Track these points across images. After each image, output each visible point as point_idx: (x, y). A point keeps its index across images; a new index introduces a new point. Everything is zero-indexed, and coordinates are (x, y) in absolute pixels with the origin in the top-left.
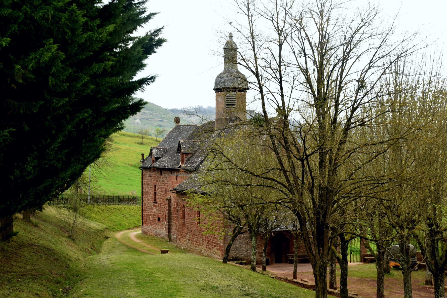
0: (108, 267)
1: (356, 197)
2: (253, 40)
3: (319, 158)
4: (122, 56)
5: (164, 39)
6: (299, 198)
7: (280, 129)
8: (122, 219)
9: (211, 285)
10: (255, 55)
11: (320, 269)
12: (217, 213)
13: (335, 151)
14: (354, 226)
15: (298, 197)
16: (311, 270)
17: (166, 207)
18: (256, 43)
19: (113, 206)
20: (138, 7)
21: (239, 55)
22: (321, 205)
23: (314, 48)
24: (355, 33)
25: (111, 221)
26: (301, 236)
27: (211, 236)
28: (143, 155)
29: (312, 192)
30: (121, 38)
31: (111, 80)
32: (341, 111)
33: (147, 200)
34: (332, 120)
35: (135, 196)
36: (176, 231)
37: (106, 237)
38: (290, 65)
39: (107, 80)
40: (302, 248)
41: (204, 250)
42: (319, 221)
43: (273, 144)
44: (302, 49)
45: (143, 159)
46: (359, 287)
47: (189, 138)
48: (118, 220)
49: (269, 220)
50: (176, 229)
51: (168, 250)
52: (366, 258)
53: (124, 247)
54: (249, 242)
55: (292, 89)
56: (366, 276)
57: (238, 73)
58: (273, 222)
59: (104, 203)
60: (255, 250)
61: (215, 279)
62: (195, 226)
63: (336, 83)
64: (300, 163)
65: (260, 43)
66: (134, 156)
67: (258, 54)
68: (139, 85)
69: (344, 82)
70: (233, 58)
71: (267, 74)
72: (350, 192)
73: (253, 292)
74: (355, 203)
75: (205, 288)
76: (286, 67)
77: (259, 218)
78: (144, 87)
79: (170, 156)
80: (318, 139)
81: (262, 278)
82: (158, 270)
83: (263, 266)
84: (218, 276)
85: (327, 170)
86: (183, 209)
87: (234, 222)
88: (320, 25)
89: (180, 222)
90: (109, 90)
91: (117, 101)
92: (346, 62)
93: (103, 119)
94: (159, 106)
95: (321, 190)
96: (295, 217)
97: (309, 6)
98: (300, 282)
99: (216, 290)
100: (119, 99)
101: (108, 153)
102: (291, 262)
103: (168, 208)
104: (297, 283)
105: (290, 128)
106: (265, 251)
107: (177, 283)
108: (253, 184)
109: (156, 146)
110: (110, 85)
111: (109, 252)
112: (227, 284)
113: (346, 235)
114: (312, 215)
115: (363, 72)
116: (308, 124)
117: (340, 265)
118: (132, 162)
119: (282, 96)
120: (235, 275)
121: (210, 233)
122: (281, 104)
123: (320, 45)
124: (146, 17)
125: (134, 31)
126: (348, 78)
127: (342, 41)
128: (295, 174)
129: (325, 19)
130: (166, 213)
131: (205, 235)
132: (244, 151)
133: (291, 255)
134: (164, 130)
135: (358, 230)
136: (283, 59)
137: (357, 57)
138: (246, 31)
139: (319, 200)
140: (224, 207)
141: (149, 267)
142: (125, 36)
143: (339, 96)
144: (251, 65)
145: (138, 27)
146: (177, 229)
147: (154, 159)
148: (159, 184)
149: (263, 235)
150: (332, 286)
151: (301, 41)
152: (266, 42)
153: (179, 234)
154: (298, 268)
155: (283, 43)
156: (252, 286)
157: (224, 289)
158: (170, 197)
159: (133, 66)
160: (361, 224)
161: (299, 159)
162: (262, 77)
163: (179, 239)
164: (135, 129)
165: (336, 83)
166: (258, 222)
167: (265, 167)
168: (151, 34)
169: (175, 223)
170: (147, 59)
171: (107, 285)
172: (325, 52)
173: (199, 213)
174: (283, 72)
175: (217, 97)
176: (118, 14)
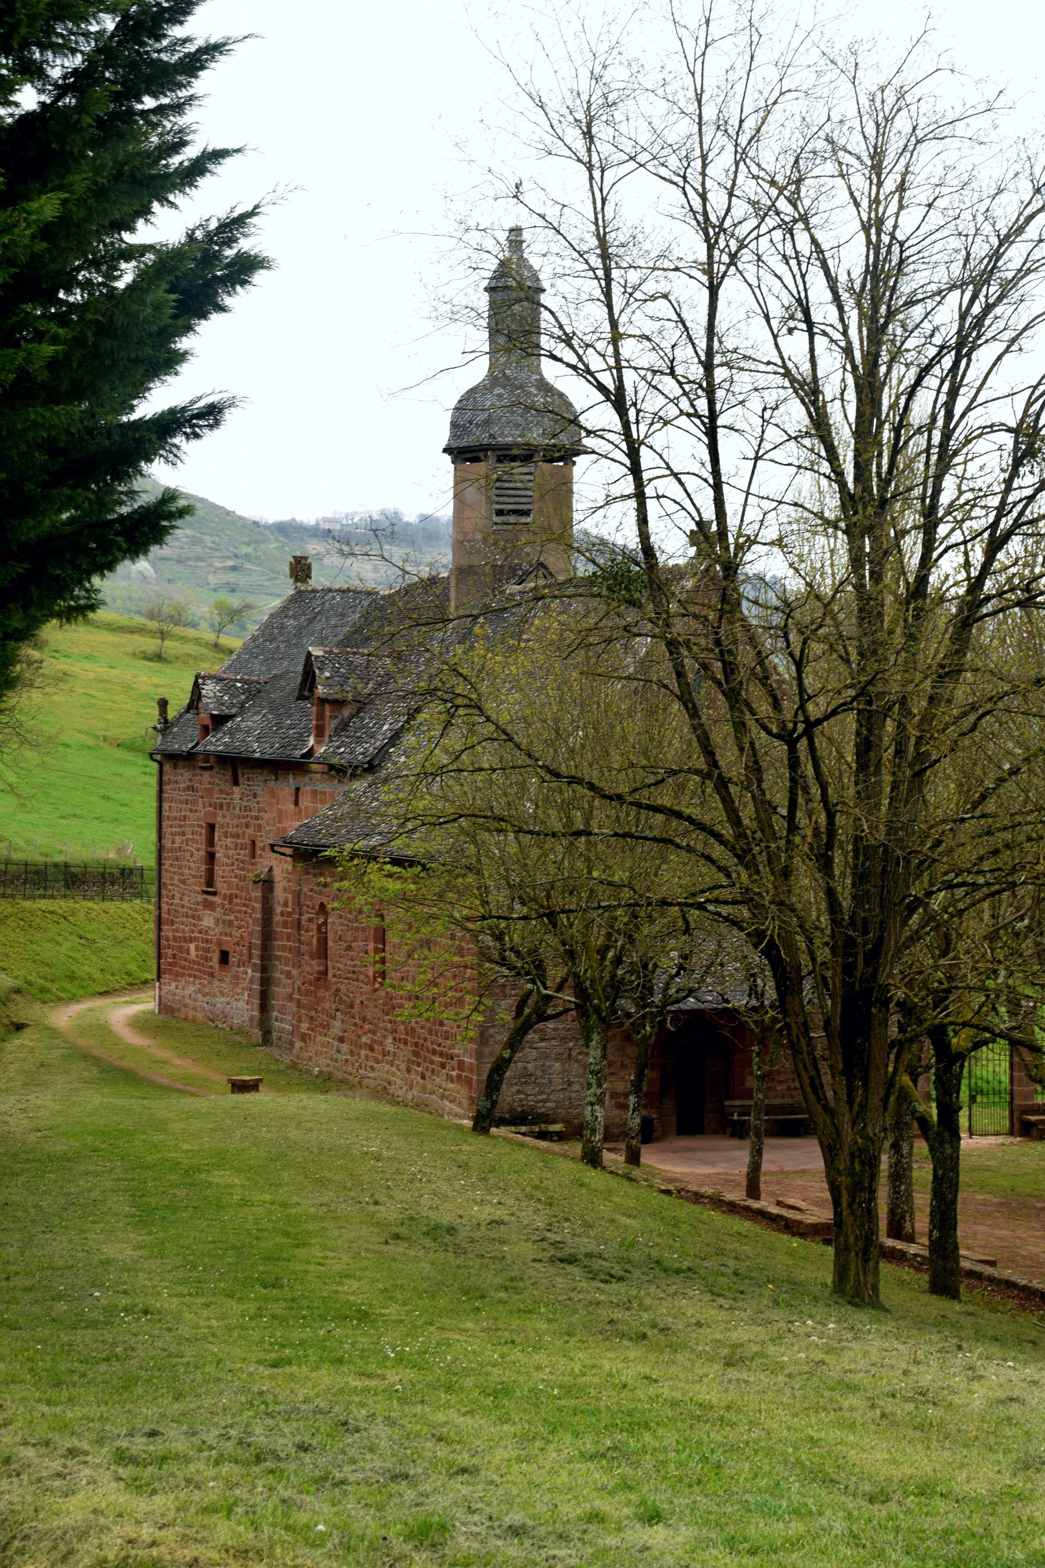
0: (24, 1143)
1: (997, 887)
2: (604, 264)
3: (858, 734)
4: (91, 321)
5: (256, 256)
6: (775, 888)
7: (706, 618)
8: (78, 955)
9: (426, 1221)
10: (614, 324)
11: (853, 1163)
12: (453, 937)
13: (918, 706)
14: (988, 996)
15: (773, 883)
16: (820, 1164)
17: (253, 909)
18: (615, 274)
19: (43, 904)
20: (154, 126)
21: (546, 320)
22: (863, 915)
23: (845, 296)
24: (1006, 240)
25: (35, 962)
26: (780, 1030)
27: (428, 1025)
28: (163, 704)
29: (825, 864)
30: (89, 249)
31: (48, 414)
32: (946, 551)
33: (180, 881)
34: (908, 583)
35: (130, 863)
36: (292, 1007)
37: (12, 1023)
38: (752, 365)
39: (33, 417)
40: (781, 1078)
41: (399, 1082)
42: (851, 976)
43: (680, 674)
44: (799, 300)
45: (166, 721)
46: (1004, 1232)
47: (347, 642)
48: (64, 959)
49: (656, 966)
50: (290, 997)
51: (261, 1080)
52: (1032, 1118)
53: (83, 1064)
54: (574, 1053)
55: (757, 458)
56: (1028, 1191)
57: (546, 388)
58: (672, 977)
59: (9, 892)
60: (600, 1086)
61: (445, 1198)
62: (368, 988)
63: (929, 439)
64: (780, 749)
65: (633, 277)
66: (129, 707)
67: (623, 319)
68: (159, 438)
69: (959, 434)
70: (529, 332)
71: (661, 401)
72: (975, 864)
73: (592, 1248)
74: (993, 908)
75: (403, 1231)
76: (734, 371)
77: (618, 961)
78: (178, 447)
79: (271, 710)
80: (854, 657)
81: (626, 1195)
82: (220, 1159)
83: (629, 1148)
84: (457, 1187)
85: (888, 778)
86: (321, 921)
87: (518, 974)
88: (870, 207)
89: (308, 969)
90: (40, 456)
91: (70, 498)
92: (969, 355)
93: (20, 568)
94: (230, 508)
95: (861, 858)
96: (756, 958)
97: (827, 128)
98: (774, 1210)
99: (448, 1239)
100: (80, 491)
101: (25, 696)
102: (738, 1131)
103: (259, 916)
104: (762, 1215)
105: (746, 612)
106: (637, 1086)
107: (294, 1211)
108: (596, 831)
109: (216, 669)
110: (45, 435)
111: (25, 1085)
112: (489, 1218)
113: (956, 1033)
114: (824, 954)
115: (1037, 393)
116: (818, 597)
117: (932, 1149)
118: (120, 731)
119: (717, 487)
120: (521, 1180)
121: (426, 1015)
122: (709, 513)
123: (868, 287)
124: (186, 164)
125: (140, 223)
126: (976, 419)
127: (956, 269)
128: (764, 794)
129: (890, 184)
130: (251, 934)
131: (403, 1023)
132: (561, 697)
133: (737, 1103)
134: (248, 607)
135: (1003, 1010)
136: (721, 342)
137: (1014, 334)
138: (580, 226)
139: (854, 897)
140: (484, 918)
141: (186, 1146)
142: (104, 242)
143: (937, 491)
144: (595, 363)
145: (156, 206)
146: (295, 996)
147: (208, 722)
148: (228, 820)
149: (632, 1024)
150: (897, 1230)
151: (795, 269)
152: (656, 273)
153: (304, 1017)
154: (766, 1156)
155: (723, 277)
156: (587, 1225)
157: (477, 1235)
158: (271, 870)
159: (136, 361)
160: (1011, 989)
161: (778, 737)
162: (638, 411)
163: (304, 1038)
164: (130, 598)
165: (929, 439)
166: (613, 976)
167: (644, 762)
168: (209, 236)
169: (289, 975)
170: (190, 335)
171: (19, 1214)
172: (891, 315)
173: (381, 935)
174: (720, 394)
175: (461, 487)
176: (76, 151)
